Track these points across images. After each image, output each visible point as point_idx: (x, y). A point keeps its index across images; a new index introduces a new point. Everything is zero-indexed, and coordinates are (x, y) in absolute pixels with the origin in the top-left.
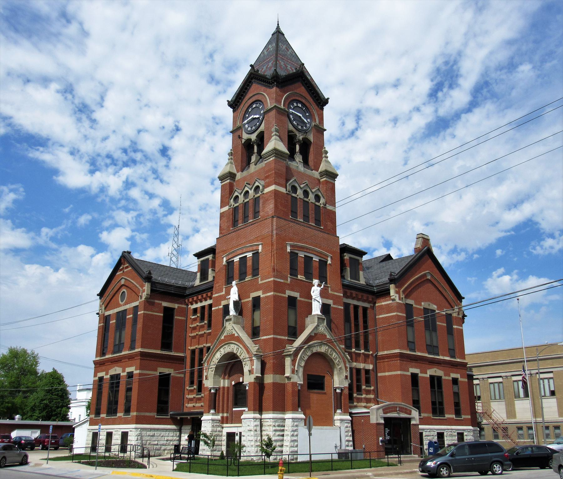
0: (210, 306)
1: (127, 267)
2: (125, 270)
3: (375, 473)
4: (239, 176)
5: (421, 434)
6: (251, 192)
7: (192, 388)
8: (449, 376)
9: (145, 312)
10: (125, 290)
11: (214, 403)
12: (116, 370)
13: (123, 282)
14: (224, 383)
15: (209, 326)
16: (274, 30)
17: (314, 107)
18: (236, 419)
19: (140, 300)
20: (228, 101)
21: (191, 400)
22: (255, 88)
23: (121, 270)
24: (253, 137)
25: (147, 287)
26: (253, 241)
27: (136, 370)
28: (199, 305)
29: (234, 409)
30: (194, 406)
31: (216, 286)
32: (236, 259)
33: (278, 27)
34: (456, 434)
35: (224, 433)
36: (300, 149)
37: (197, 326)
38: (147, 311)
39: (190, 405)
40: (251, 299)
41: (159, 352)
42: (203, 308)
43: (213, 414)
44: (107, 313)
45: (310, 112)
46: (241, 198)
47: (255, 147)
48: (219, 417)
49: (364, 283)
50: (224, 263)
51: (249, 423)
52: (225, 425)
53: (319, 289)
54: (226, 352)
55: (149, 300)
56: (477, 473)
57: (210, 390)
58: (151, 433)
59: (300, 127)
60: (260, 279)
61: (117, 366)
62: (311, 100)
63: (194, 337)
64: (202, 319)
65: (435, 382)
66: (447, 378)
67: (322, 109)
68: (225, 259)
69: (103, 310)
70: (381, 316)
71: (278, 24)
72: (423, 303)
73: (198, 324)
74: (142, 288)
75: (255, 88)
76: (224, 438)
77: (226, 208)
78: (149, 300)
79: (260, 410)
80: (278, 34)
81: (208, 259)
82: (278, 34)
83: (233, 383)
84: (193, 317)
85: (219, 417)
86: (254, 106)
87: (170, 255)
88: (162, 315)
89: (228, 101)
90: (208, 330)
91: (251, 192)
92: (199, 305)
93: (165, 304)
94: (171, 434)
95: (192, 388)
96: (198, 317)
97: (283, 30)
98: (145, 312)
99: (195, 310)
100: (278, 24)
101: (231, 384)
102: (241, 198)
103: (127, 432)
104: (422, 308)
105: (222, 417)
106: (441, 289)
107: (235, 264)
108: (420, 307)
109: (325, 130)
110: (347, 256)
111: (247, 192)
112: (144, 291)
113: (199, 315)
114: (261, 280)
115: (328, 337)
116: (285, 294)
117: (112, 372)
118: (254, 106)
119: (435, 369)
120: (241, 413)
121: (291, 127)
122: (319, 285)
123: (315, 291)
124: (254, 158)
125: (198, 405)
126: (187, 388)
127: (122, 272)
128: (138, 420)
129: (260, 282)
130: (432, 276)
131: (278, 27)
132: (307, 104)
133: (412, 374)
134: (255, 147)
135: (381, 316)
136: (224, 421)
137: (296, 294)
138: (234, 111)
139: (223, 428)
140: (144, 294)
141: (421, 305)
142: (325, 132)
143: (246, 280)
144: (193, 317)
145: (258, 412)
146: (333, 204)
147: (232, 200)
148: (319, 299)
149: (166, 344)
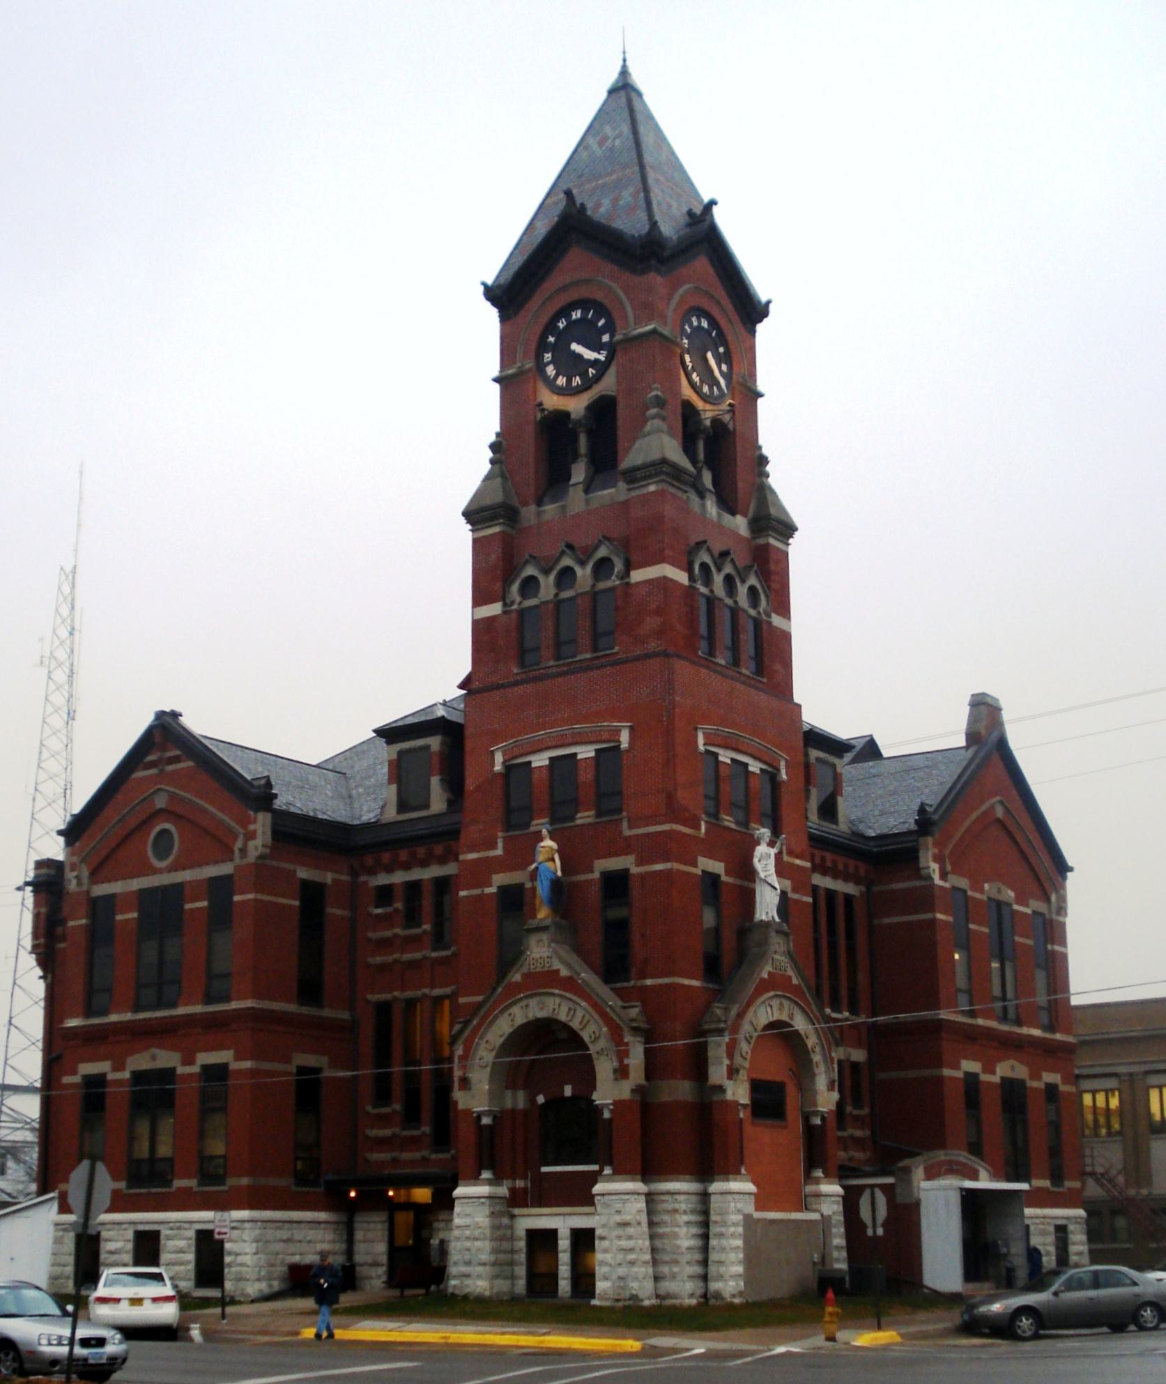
0: (442, 885)
1: (177, 760)
2: (170, 768)
3: (912, 1329)
4: (529, 513)
5: (1028, 1226)
6: (584, 574)
7: (387, 1110)
8: (1039, 1078)
9: (260, 896)
10: (167, 826)
11: (493, 1150)
12: (154, 1058)
13: (161, 802)
14: (515, 1098)
15: (439, 939)
16: (611, 77)
17: (732, 329)
18: (579, 1193)
19: (237, 861)
20: (484, 284)
21: (382, 1143)
22: (578, 266)
23: (152, 765)
24: (576, 406)
25: (262, 824)
26: (600, 716)
27: (238, 1058)
28: (399, 877)
29: (545, 1169)
30: (394, 1160)
31: (472, 832)
32: (540, 760)
33: (624, 72)
34: (1052, 1229)
35: (521, 1233)
36: (706, 457)
37: (396, 936)
38: (262, 892)
39: (375, 1156)
40: (596, 875)
41: (292, 1008)
42: (414, 888)
43: (490, 1182)
44: (100, 890)
45: (725, 344)
46: (547, 585)
47: (583, 440)
48: (503, 1190)
49: (847, 831)
50: (498, 767)
51: (618, 1206)
52: (516, 1211)
53: (773, 851)
54: (531, 1016)
55: (268, 862)
56: (1105, 1329)
57: (479, 1118)
58: (284, 1234)
59: (706, 389)
60: (625, 824)
61: (157, 1047)
62: (729, 307)
63: (382, 968)
64: (412, 917)
65: (1012, 1091)
66: (1035, 1084)
67: (753, 332)
68: (499, 758)
69: (85, 881)
70: (887, 921)
71: (624, 60)
72: (986, 886)
73: (398, 931)
74: (244, 826)
75: (578, 266)
76: (522, 1244)
77: (495, 609)
78: (268, 862)
79: (648, 1171)
80: (624, 91)
81: (427, 747)
82: (624, 91)
83: (541, 1099)
84: (379, 911)
85: (503, 1190)
86: (577, 315)
87: (46, 661)
88: (296, 903)
89: (484, 284)
90: (434, 950)
91: (584, 574)
92: (399, 877)
93: (303, 873)
94: (312, 1234)
95: (387, 1110)
96: (396, 910)
97: (639, 78)
98: (260, 896)
99: (385, 894)
100: (624, 60)
101: (532, 1100)
102: (547, 585)
103: (157, 1233)
104: (984, 898)
105: (512, 1190)
106: (1024, 845)
107: (536, 776)
108: (978, 896)
109: (761, 395)
110: (814, 754)
111: (567, 573)
112: (251, 836)
113: (399, 905)
114: (630, 827)
115: (795, 981)
116: (696, 866)
117: (142, 1061)
118: (577, 315)
119: (1012, 1062)
120: (593, 1178)
121: (687, 392)
122: (771, 844)
123: (764, 858)
124: (579, 473)
125: (406, 1156)
126: (369, 1109)
127: (153, 771)
128: (254, 1200)
129: (627, 832)
130: (1007, 810)
131: (624, 72)
132: (723, 322)
133: (966, 1074)
134: (583, 440)
135: (887, 921)
136: (517, 1199)
137: (717, 867)
138: (504, 318)
139: (512, 1217)
140: (251, 844)
141: (982, 891)
142: (760, 401)
143: (579, 822)
144: (379, 911)
145: (639, 1177)
146: (783, 607)
147: (515, 588)
148: (774, 880)
149: (310, 991)
